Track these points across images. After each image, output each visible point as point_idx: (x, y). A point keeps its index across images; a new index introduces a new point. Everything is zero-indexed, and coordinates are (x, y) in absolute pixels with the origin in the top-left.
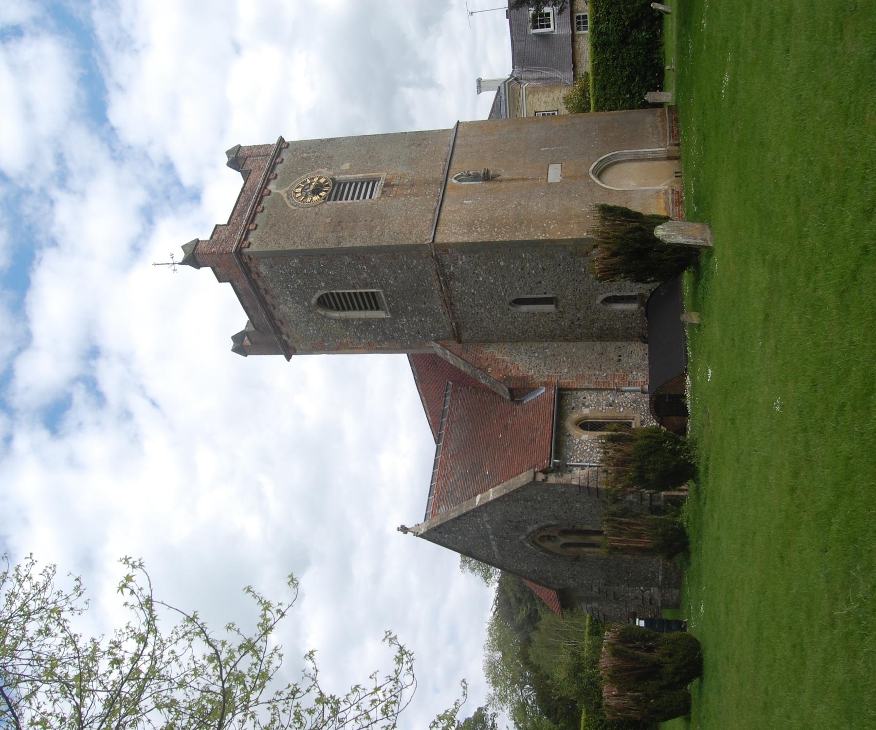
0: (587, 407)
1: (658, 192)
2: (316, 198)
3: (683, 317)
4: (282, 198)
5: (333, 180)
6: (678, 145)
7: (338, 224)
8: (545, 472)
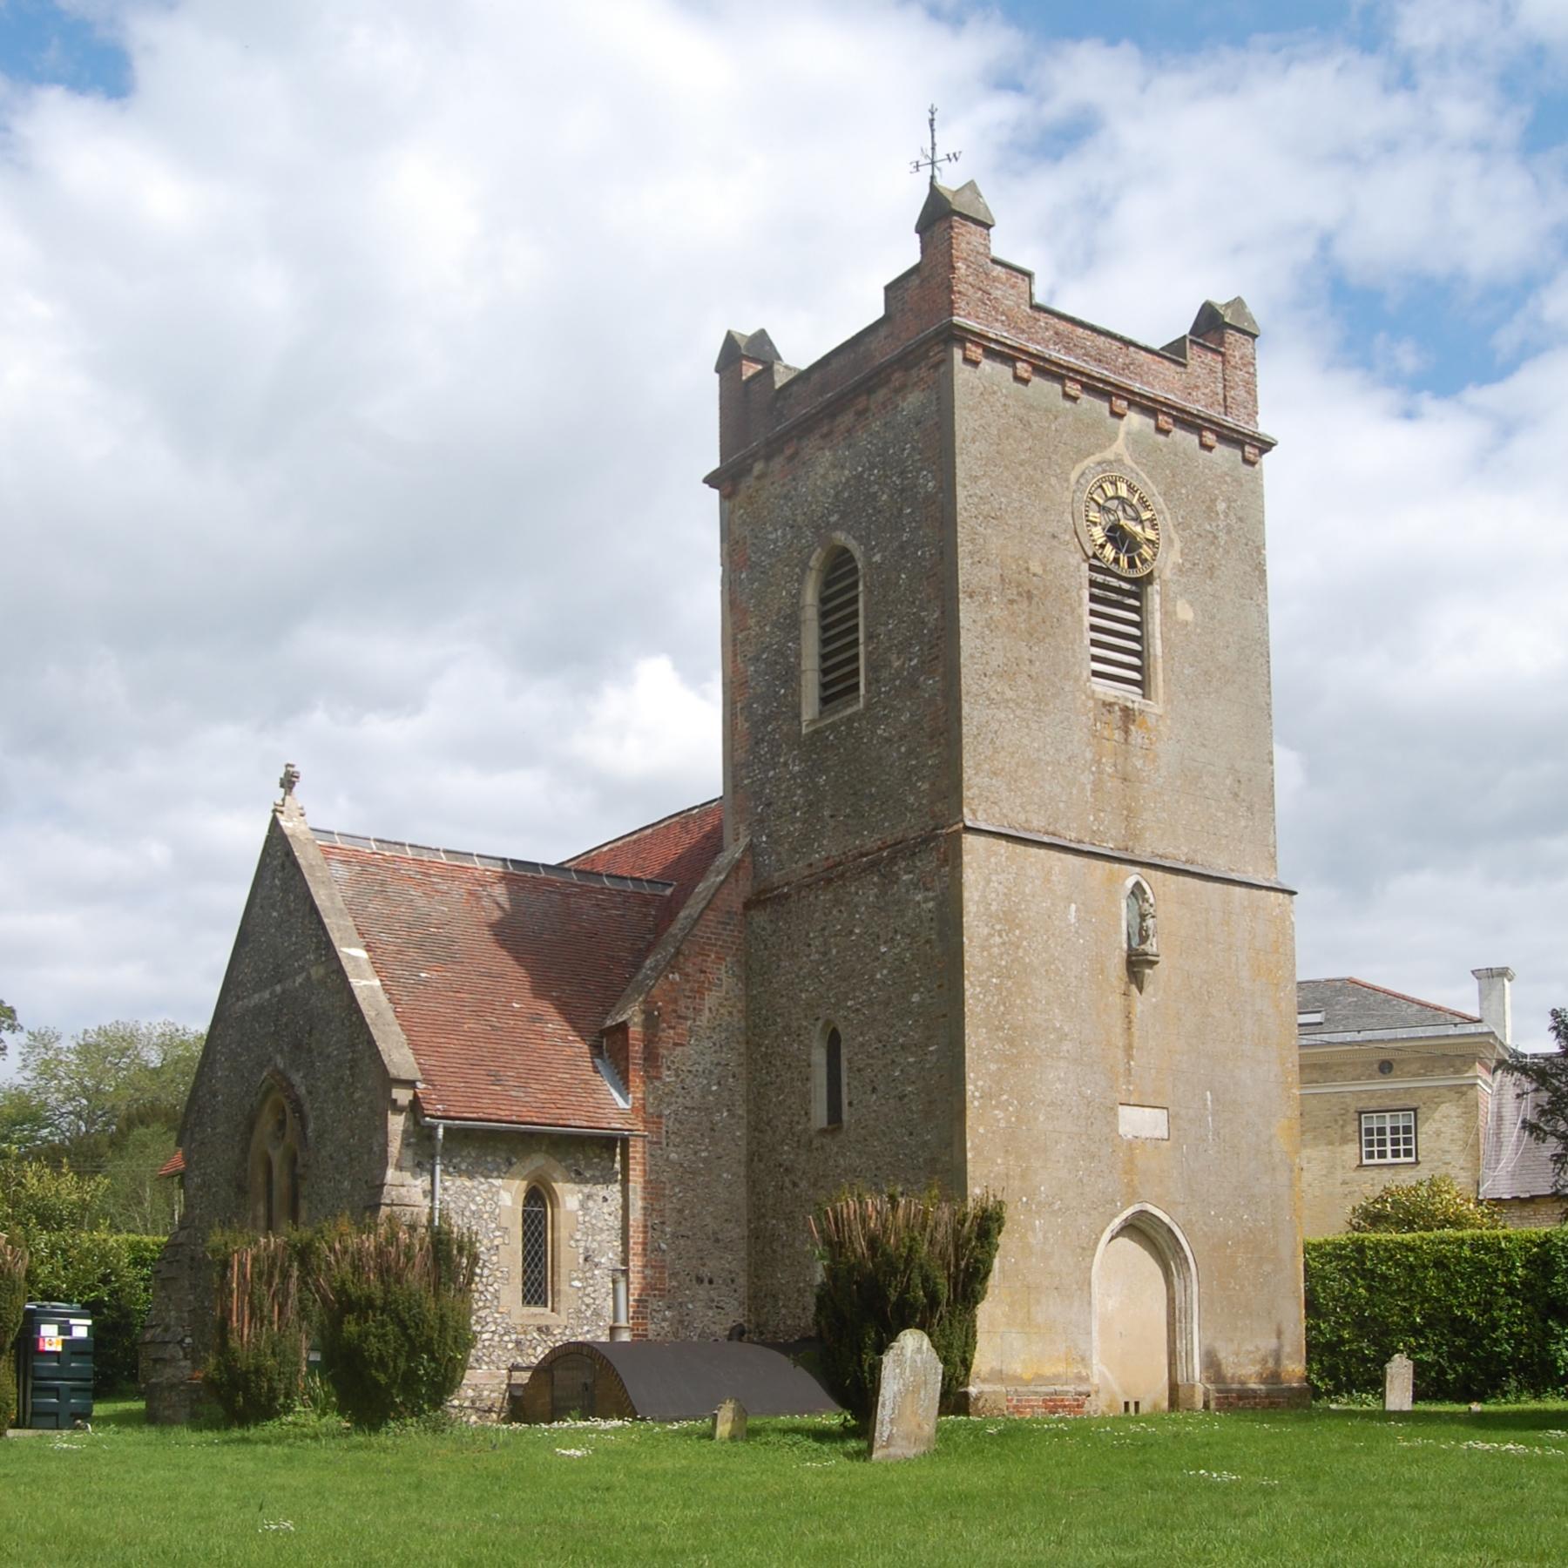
0: (583, 1206)
1: (1084, 1360)
2: (1099, 534)
5: (1148, 579)
8: (415, 1107)
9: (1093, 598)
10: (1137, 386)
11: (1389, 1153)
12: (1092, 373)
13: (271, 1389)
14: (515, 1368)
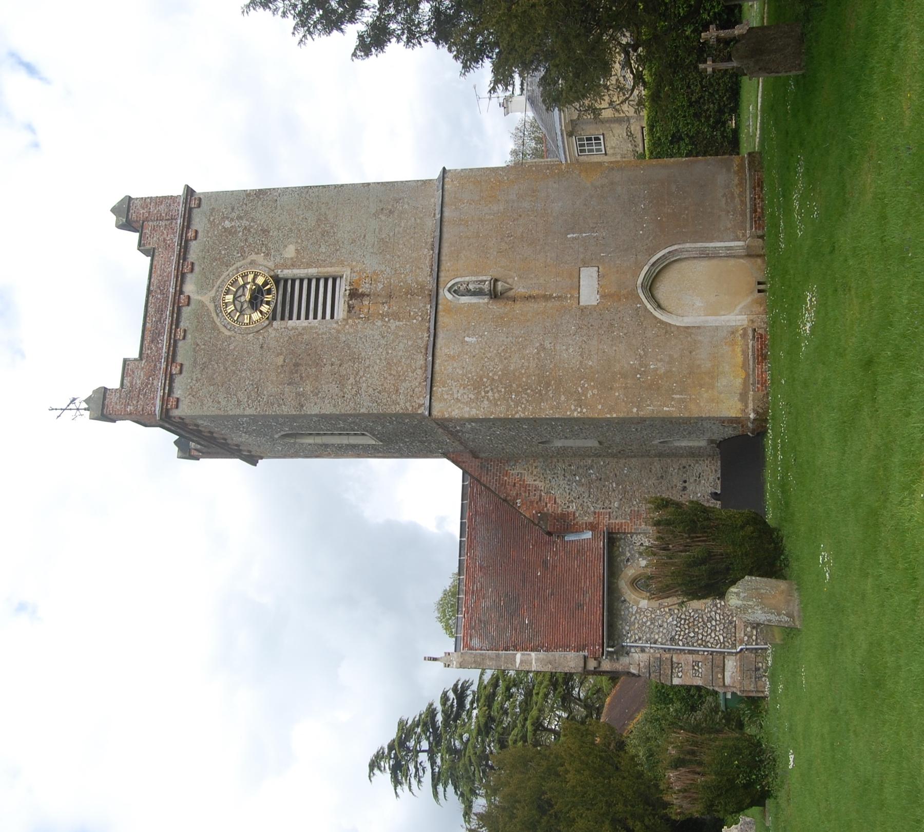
2: (256, 316)
5: (277, 280)
6: (762, 237)
9: (291, 318)
10: (172, 290)
12: (166, 312)
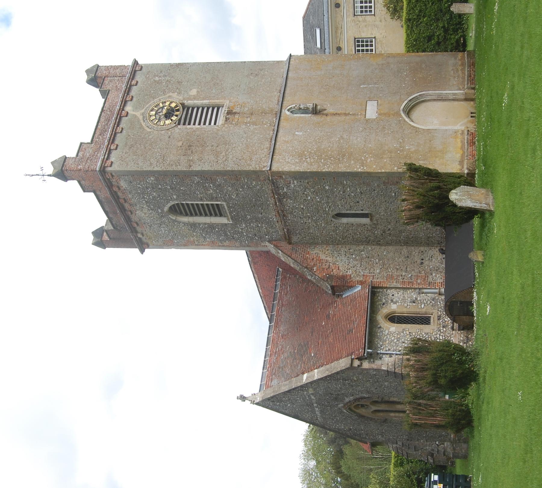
0: (395, 303)
2: (168, 122)
3: (471, 256)
4: (139, 120)
5: (183, 104)
6: (474, 89)
7: (189, 148)
8: (360, 359)
9: (189, 124)
10: (118, 108)
11: (370, 5)
12: (112, 123)
13: (460, 411)
14: (453, 328)
